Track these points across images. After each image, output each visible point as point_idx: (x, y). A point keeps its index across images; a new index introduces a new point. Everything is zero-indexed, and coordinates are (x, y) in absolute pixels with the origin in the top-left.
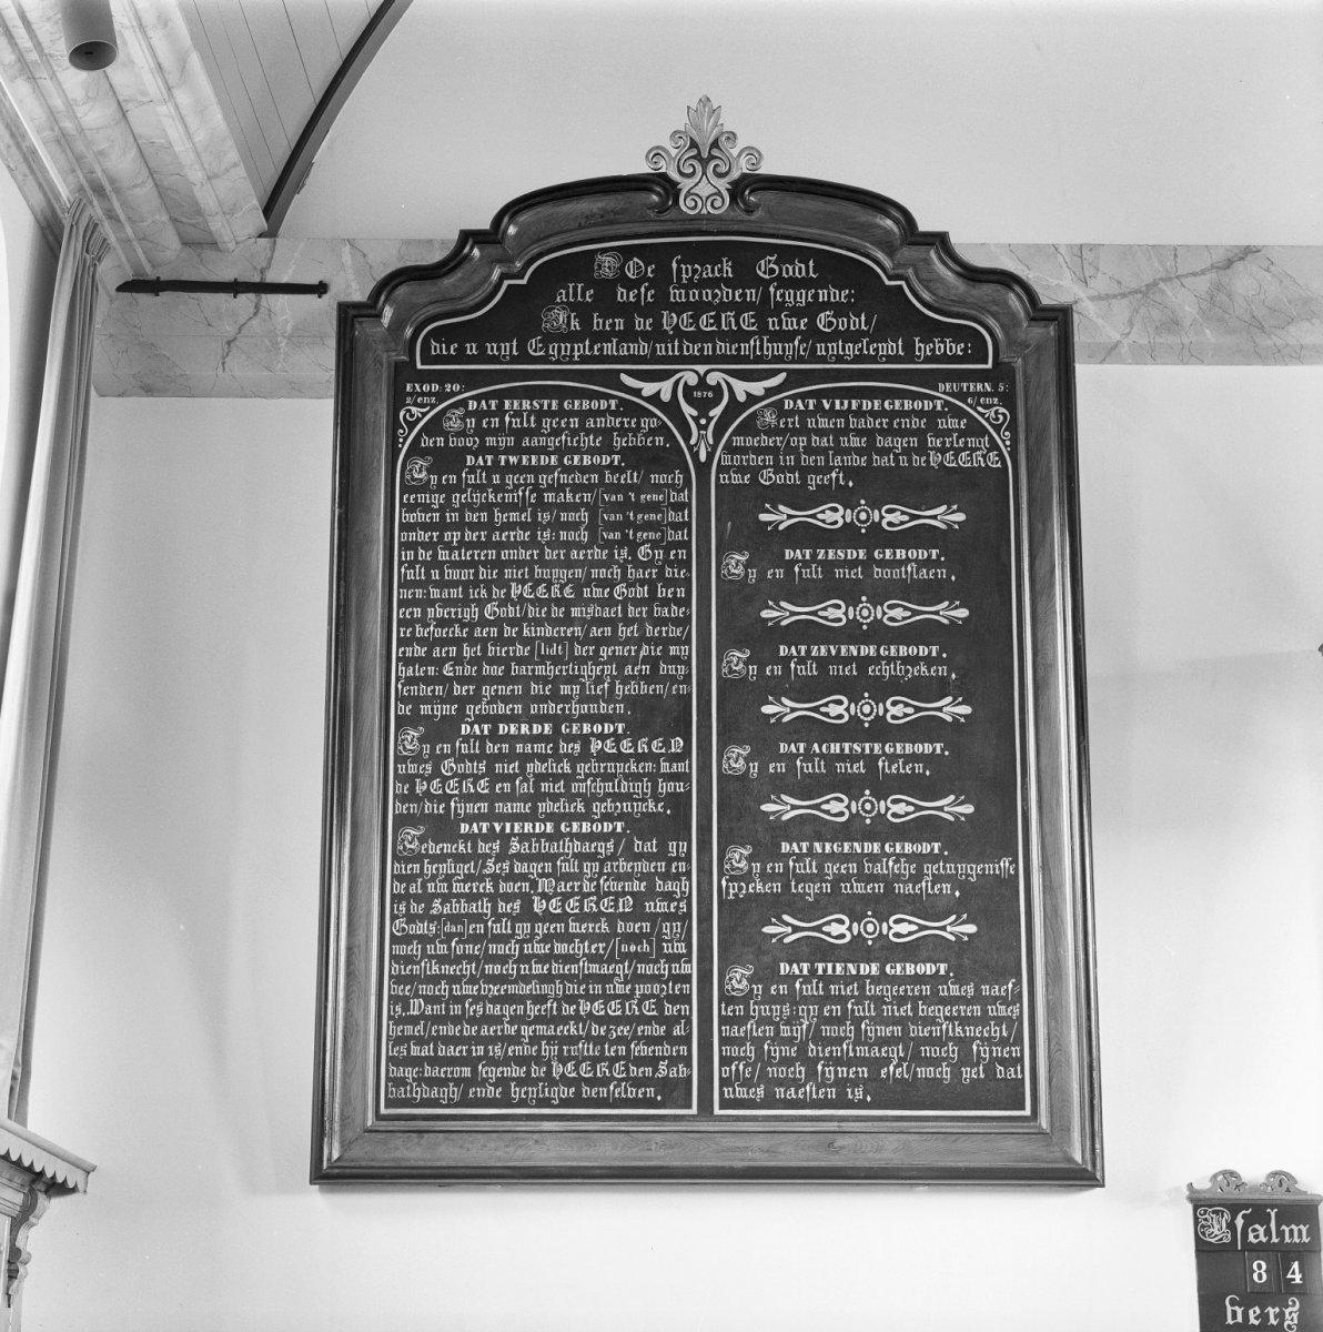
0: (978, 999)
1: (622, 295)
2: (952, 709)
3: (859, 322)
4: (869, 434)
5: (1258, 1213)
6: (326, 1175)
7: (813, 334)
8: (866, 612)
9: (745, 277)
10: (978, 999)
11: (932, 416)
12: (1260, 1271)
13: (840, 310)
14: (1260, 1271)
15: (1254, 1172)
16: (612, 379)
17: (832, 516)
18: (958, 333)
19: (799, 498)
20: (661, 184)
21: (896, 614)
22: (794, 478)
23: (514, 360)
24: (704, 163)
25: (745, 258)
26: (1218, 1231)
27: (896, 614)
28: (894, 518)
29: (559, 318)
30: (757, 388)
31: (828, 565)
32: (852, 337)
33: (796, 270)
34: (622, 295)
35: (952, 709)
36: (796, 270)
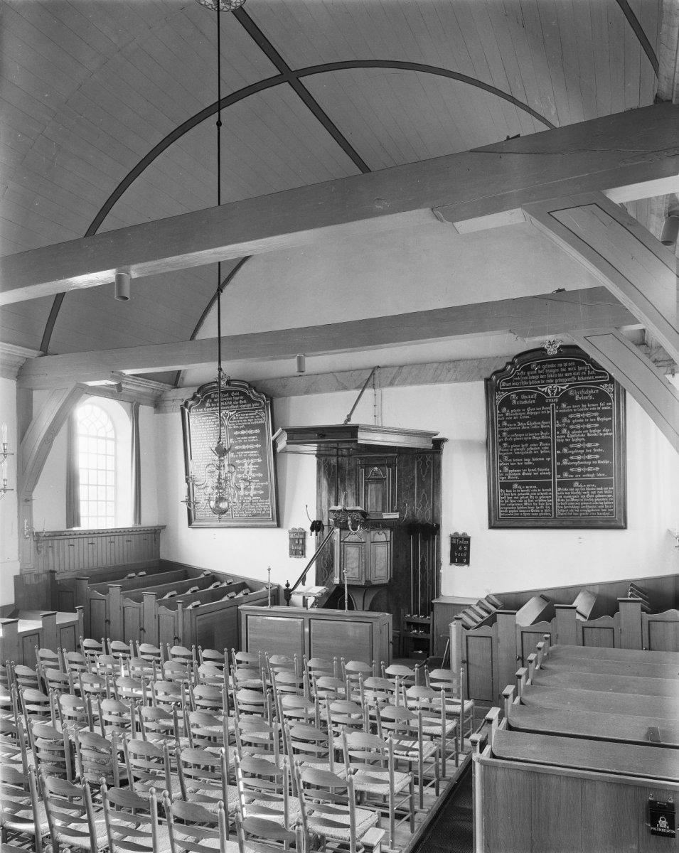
0: (264, 502)
1: (215, 400)
2: (259, 460)
3: (245, 402)
4: (247, 419)
5: (461, 539)
6: (491, 527)
7: (239, 404)
8: (248, 447)
9: (230, 396)
10: (264, 502)
11: (255, 416)
12: (460, 548)
13: (243, 400)
14: (460, 548)
15: (460, 533)
16: (536, 389)
17: (243, 432)
18: (258, 402)
19: (239, 430)
20: (543, 349)
21: (252, 447)
22: (237, 427)
23: (575, 381)
24: (552, 345)
25: (230, 392)
26: (292, 536)
27: (252, 447)
28: (251, 432)
29: (207, 405)
30: (232, 413)
31: (243, 440)
32: (244, 404)
33: (237, 394)
34: (215, 400)
35: (259, 460)
36: (237, 394)
